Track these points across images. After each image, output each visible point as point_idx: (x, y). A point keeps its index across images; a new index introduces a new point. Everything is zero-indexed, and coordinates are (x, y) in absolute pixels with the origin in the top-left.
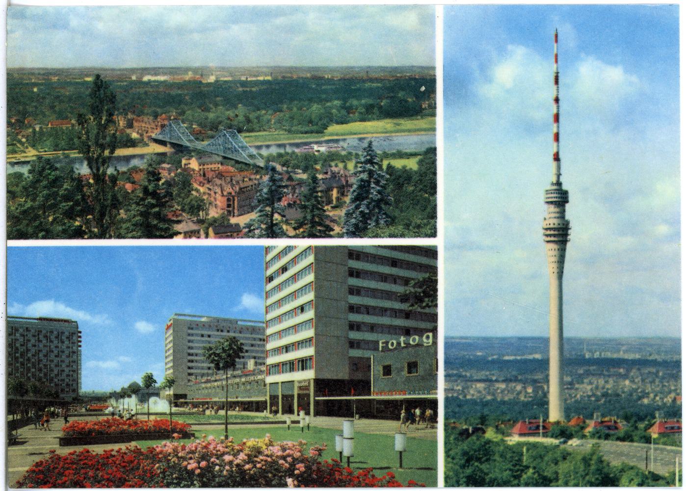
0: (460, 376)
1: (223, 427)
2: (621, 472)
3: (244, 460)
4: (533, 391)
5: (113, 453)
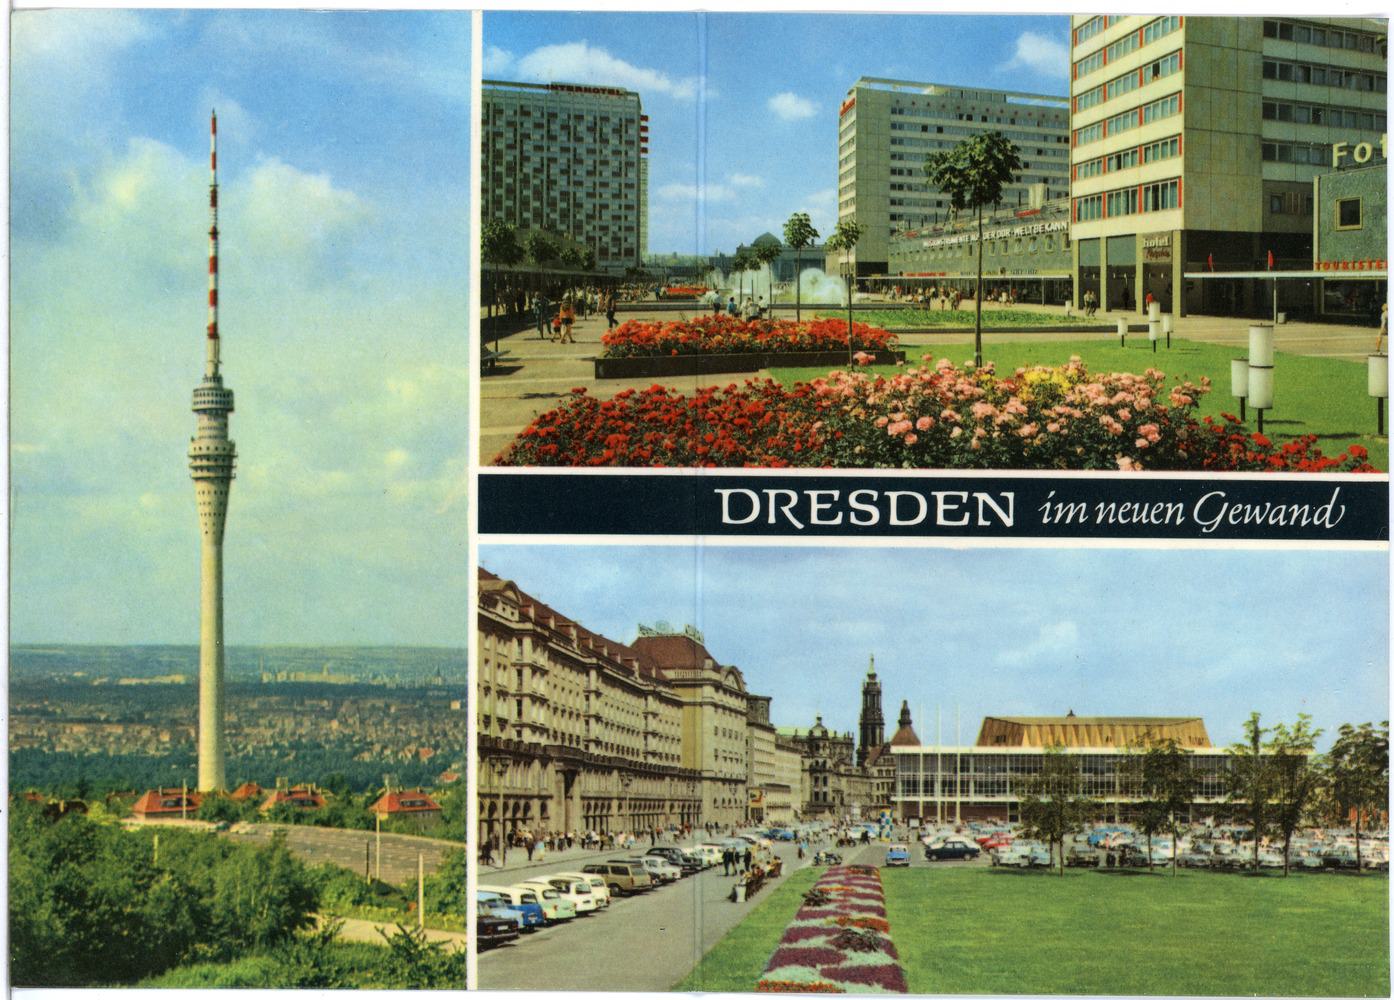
0: (44, 713)
1: (972, 337)
2: (322, 879)
3: (1018, 415)
4: (171, 739)
5: (717, 395)
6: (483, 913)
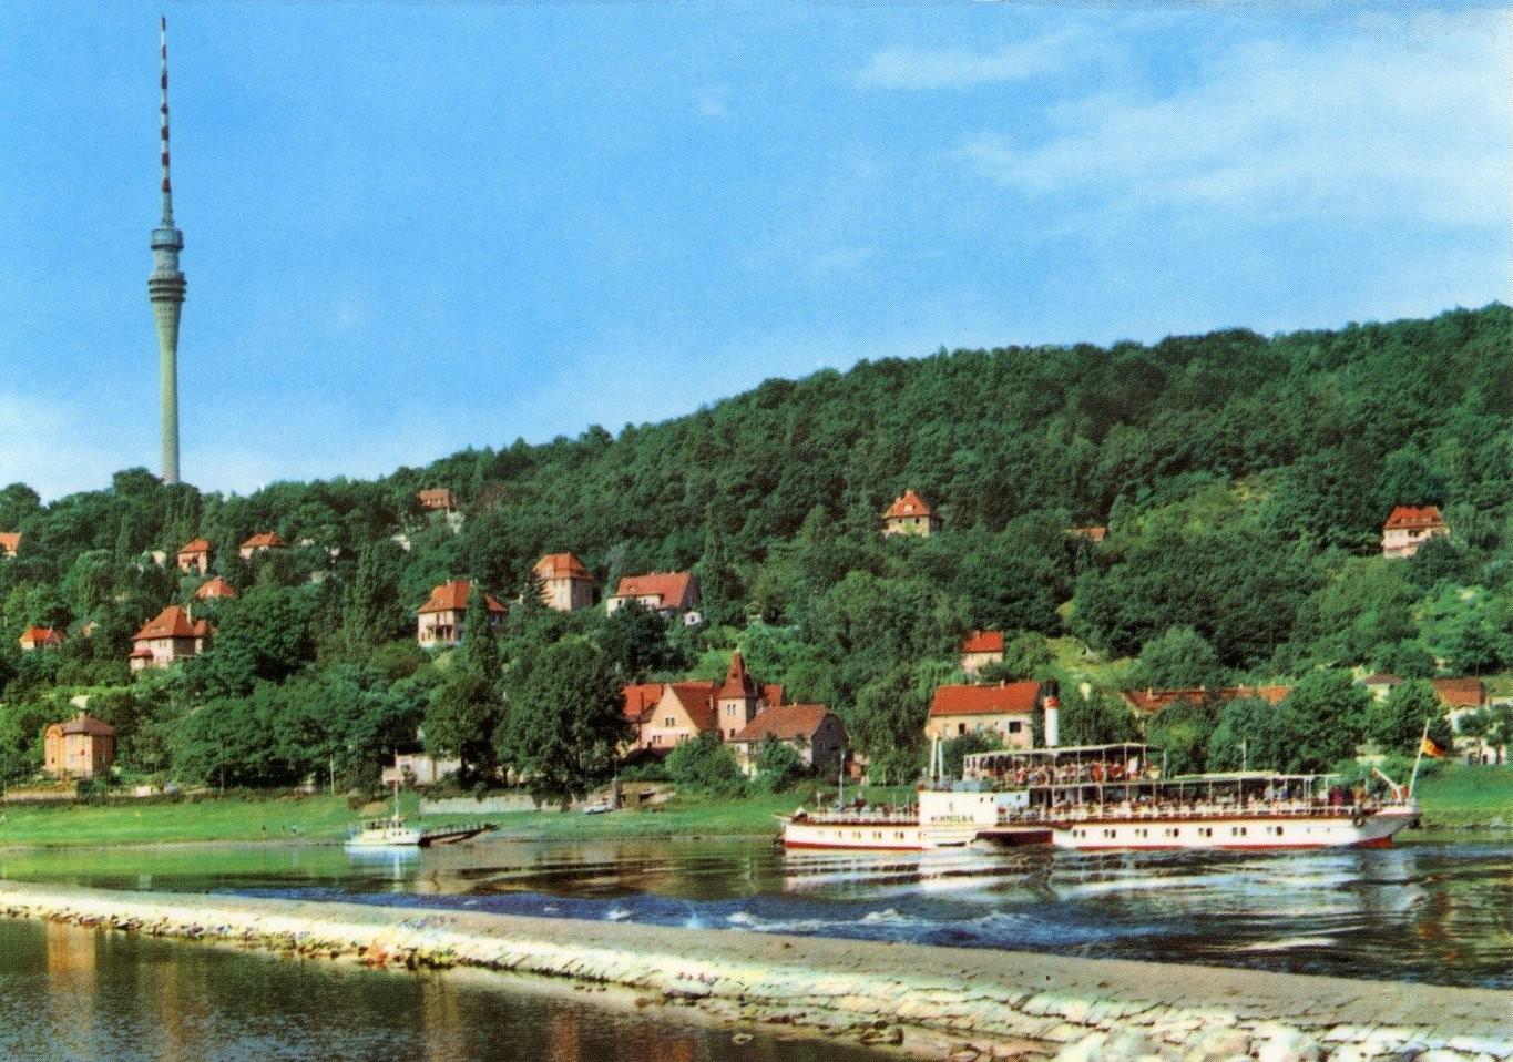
6: (225, 595)
